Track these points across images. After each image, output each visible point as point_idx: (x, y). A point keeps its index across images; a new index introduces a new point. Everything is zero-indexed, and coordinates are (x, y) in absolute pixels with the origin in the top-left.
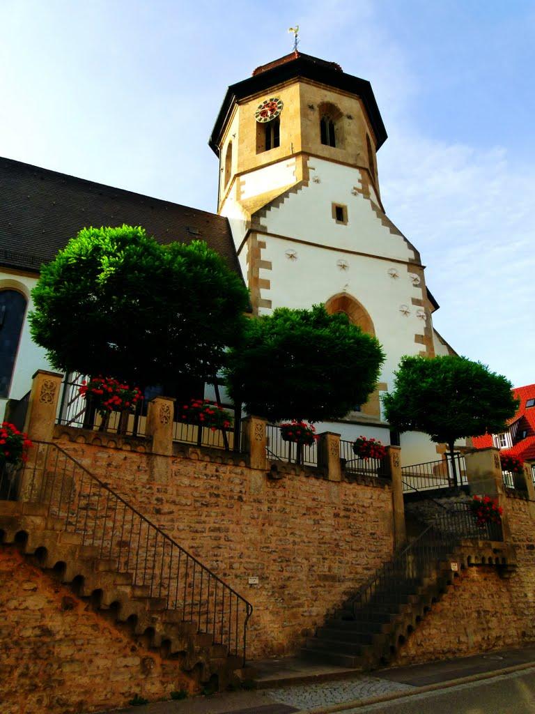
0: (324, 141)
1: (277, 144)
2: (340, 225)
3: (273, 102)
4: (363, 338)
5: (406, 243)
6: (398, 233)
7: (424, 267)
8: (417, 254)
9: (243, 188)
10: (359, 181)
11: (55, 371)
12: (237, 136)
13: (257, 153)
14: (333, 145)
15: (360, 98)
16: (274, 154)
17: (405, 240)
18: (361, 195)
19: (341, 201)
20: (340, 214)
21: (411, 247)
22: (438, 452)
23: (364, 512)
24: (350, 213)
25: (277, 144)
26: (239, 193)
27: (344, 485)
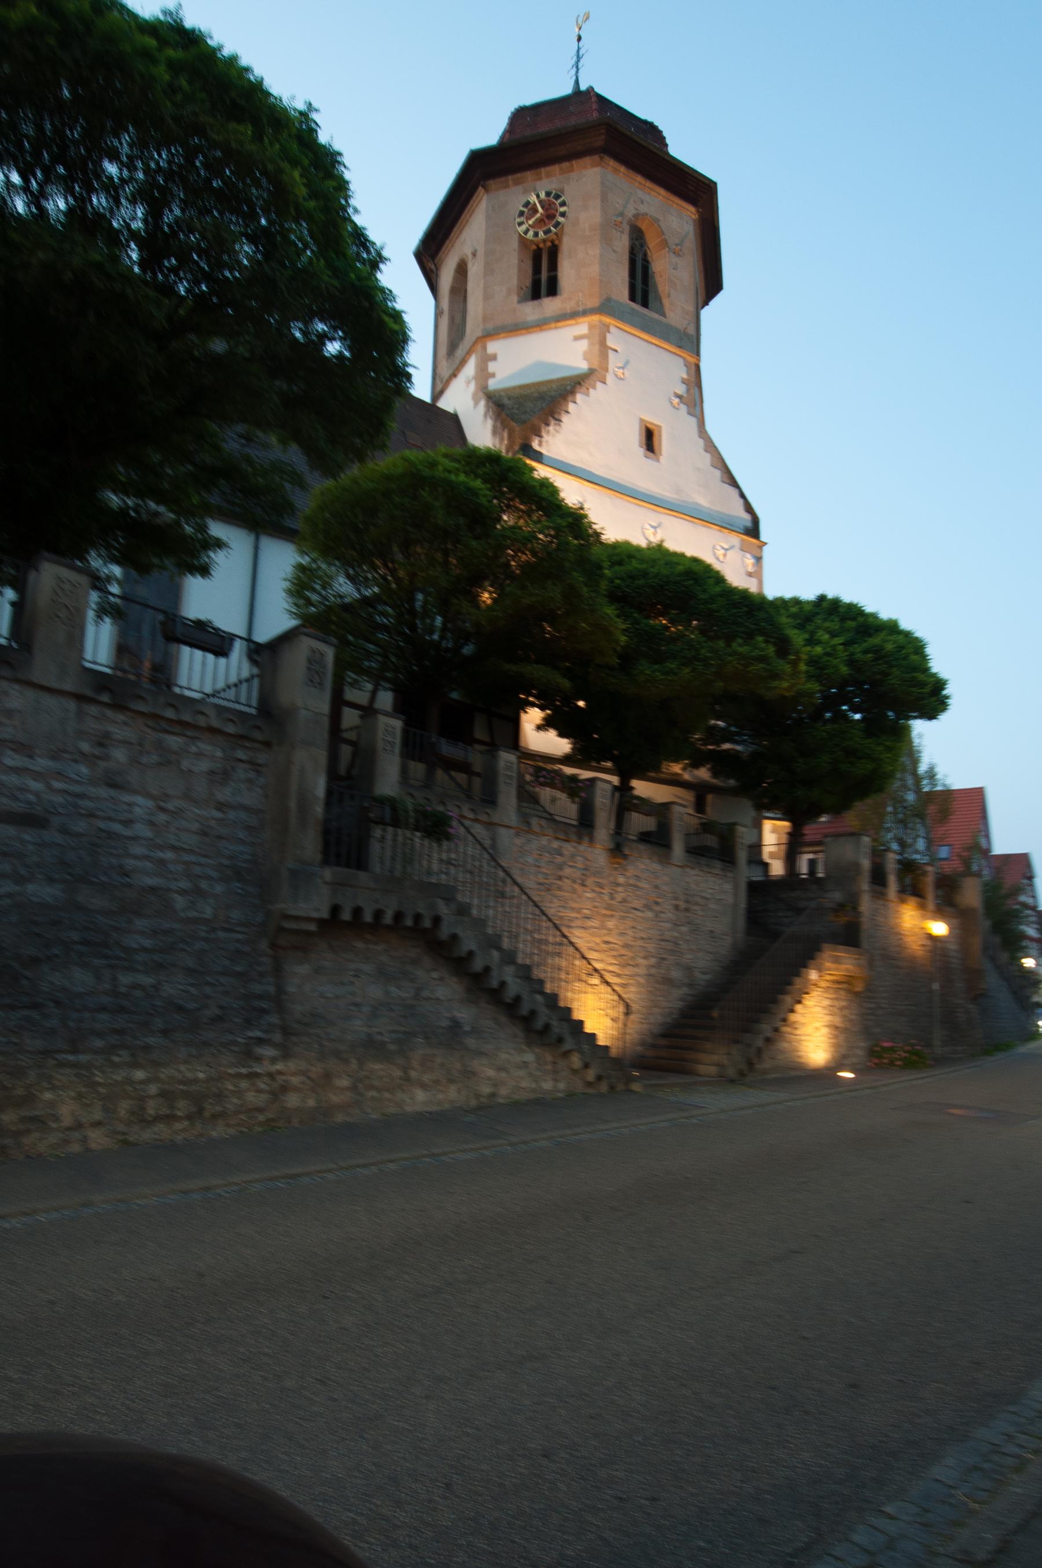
0: (632, 298)
1: (553, 290)
2: (650, 461)
3: (551, 198)
4: (614, 543)
5: (741, 501)
6: (733, 483)
7: (766, 544)
8: (756, 521)
9: (492, 367)
10: (684, 381)
11: (696, 814)
12: (481, 253)
13: (519, 302)
14: (645, 304)
15: (775, 1001)
16: (550, 305)
17: (742, 496)
18: (683, 408)
19: (652, 419)
20: (650, 439)
21: (749, 508)
22: (585, 359)
23: (687, 910)
24: (665, 442)
25: (553, 290)
26: (483, 374)
27: (688, 870)
